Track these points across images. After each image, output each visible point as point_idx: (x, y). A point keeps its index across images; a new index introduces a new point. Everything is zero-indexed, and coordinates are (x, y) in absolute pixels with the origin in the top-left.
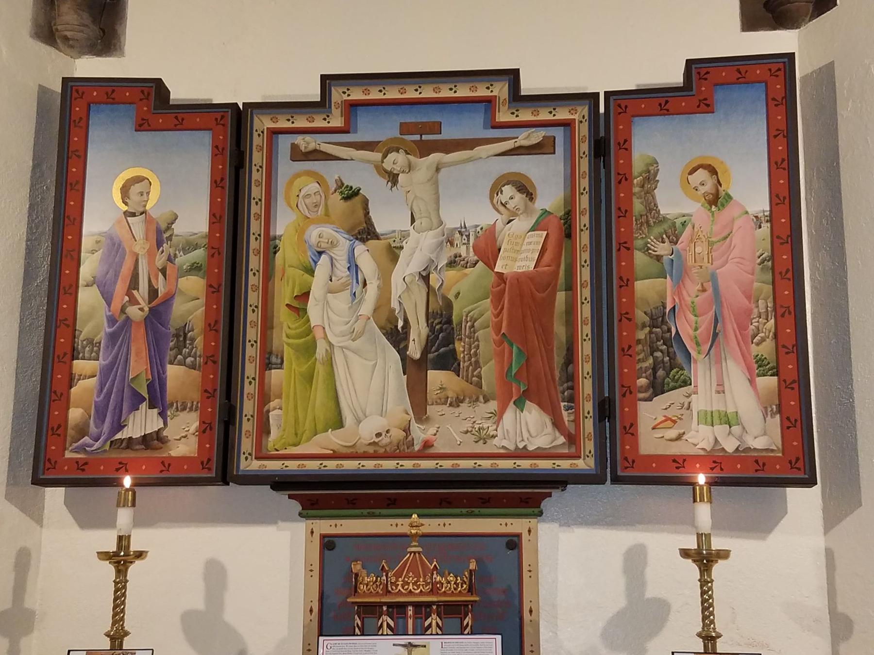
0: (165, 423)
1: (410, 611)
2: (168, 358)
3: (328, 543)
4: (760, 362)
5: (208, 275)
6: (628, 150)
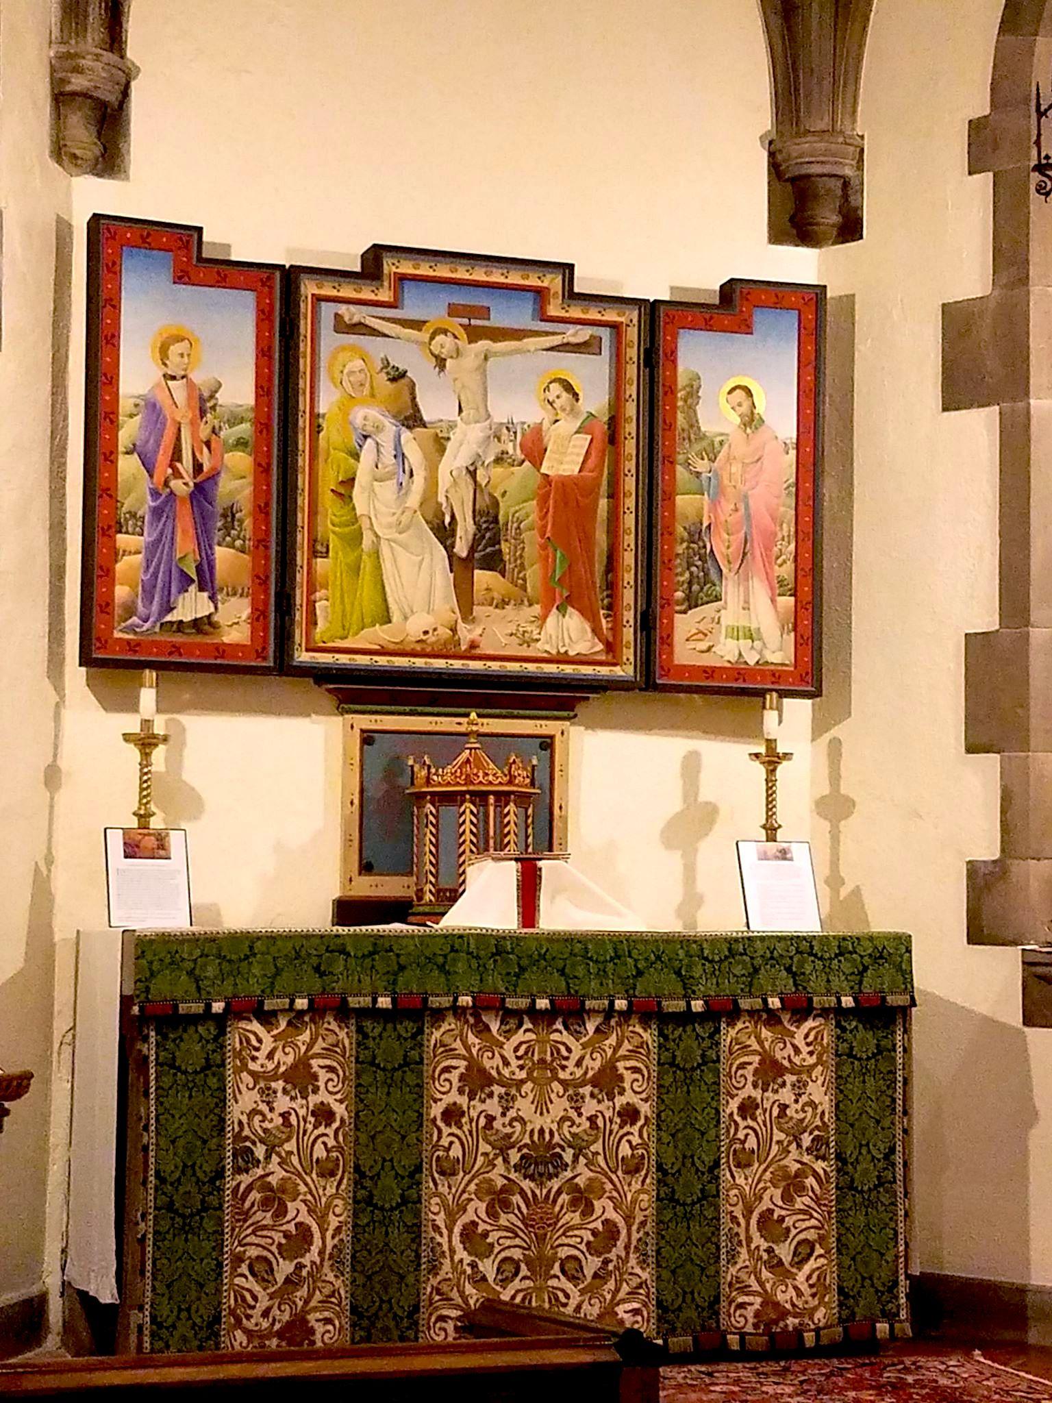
0: (216, 608)
1: (492, 799)
2: (216, 541)
3: (368, 738)
4: (781, 582)
5: (256, 453)
6: (674, 362)
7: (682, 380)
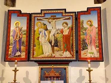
1: (52, 77)
3: (42, 69)
4: (97, 46)
6: (80, 19)
7: (81, 21)
